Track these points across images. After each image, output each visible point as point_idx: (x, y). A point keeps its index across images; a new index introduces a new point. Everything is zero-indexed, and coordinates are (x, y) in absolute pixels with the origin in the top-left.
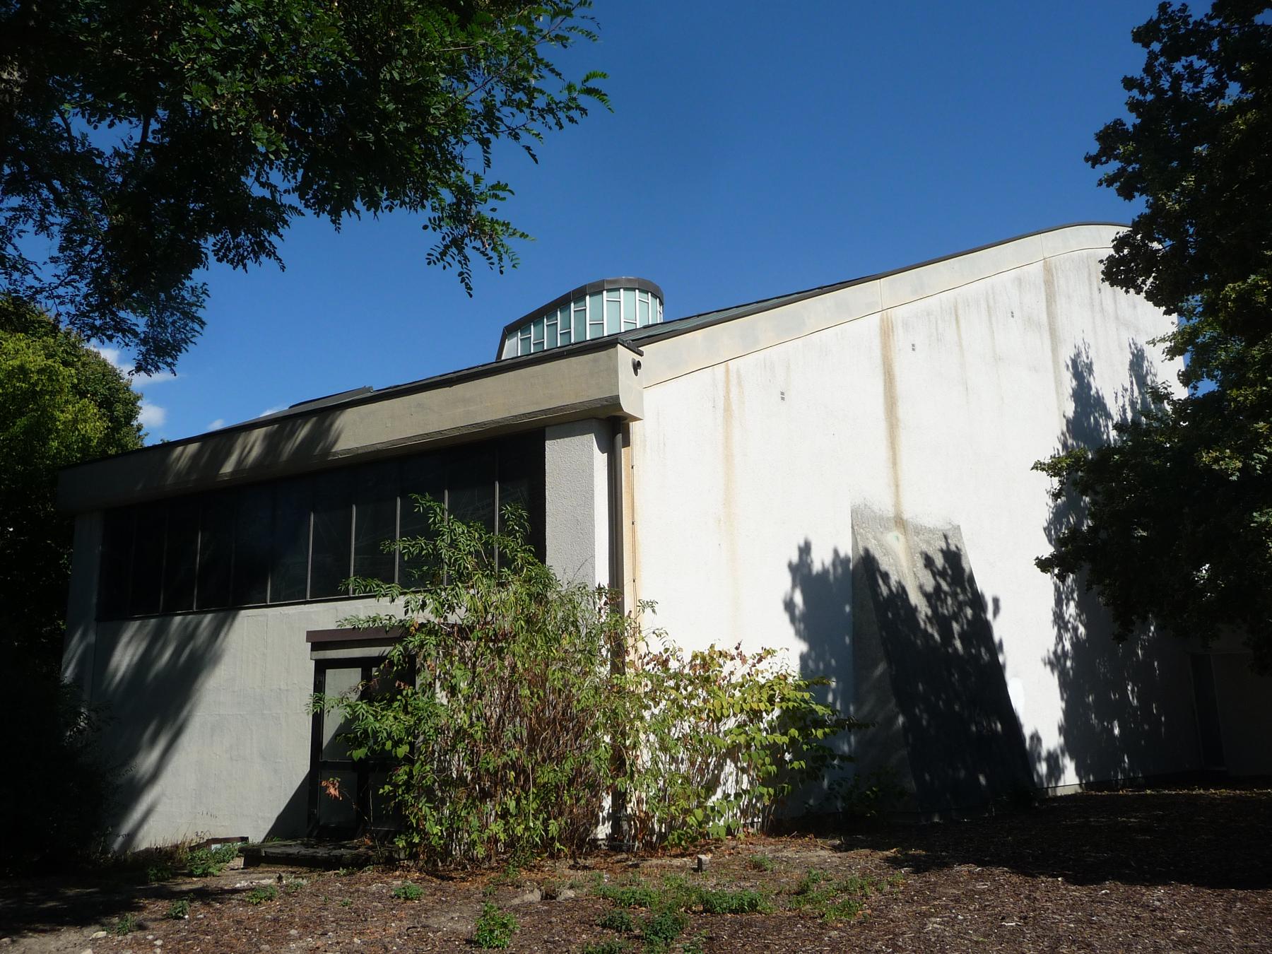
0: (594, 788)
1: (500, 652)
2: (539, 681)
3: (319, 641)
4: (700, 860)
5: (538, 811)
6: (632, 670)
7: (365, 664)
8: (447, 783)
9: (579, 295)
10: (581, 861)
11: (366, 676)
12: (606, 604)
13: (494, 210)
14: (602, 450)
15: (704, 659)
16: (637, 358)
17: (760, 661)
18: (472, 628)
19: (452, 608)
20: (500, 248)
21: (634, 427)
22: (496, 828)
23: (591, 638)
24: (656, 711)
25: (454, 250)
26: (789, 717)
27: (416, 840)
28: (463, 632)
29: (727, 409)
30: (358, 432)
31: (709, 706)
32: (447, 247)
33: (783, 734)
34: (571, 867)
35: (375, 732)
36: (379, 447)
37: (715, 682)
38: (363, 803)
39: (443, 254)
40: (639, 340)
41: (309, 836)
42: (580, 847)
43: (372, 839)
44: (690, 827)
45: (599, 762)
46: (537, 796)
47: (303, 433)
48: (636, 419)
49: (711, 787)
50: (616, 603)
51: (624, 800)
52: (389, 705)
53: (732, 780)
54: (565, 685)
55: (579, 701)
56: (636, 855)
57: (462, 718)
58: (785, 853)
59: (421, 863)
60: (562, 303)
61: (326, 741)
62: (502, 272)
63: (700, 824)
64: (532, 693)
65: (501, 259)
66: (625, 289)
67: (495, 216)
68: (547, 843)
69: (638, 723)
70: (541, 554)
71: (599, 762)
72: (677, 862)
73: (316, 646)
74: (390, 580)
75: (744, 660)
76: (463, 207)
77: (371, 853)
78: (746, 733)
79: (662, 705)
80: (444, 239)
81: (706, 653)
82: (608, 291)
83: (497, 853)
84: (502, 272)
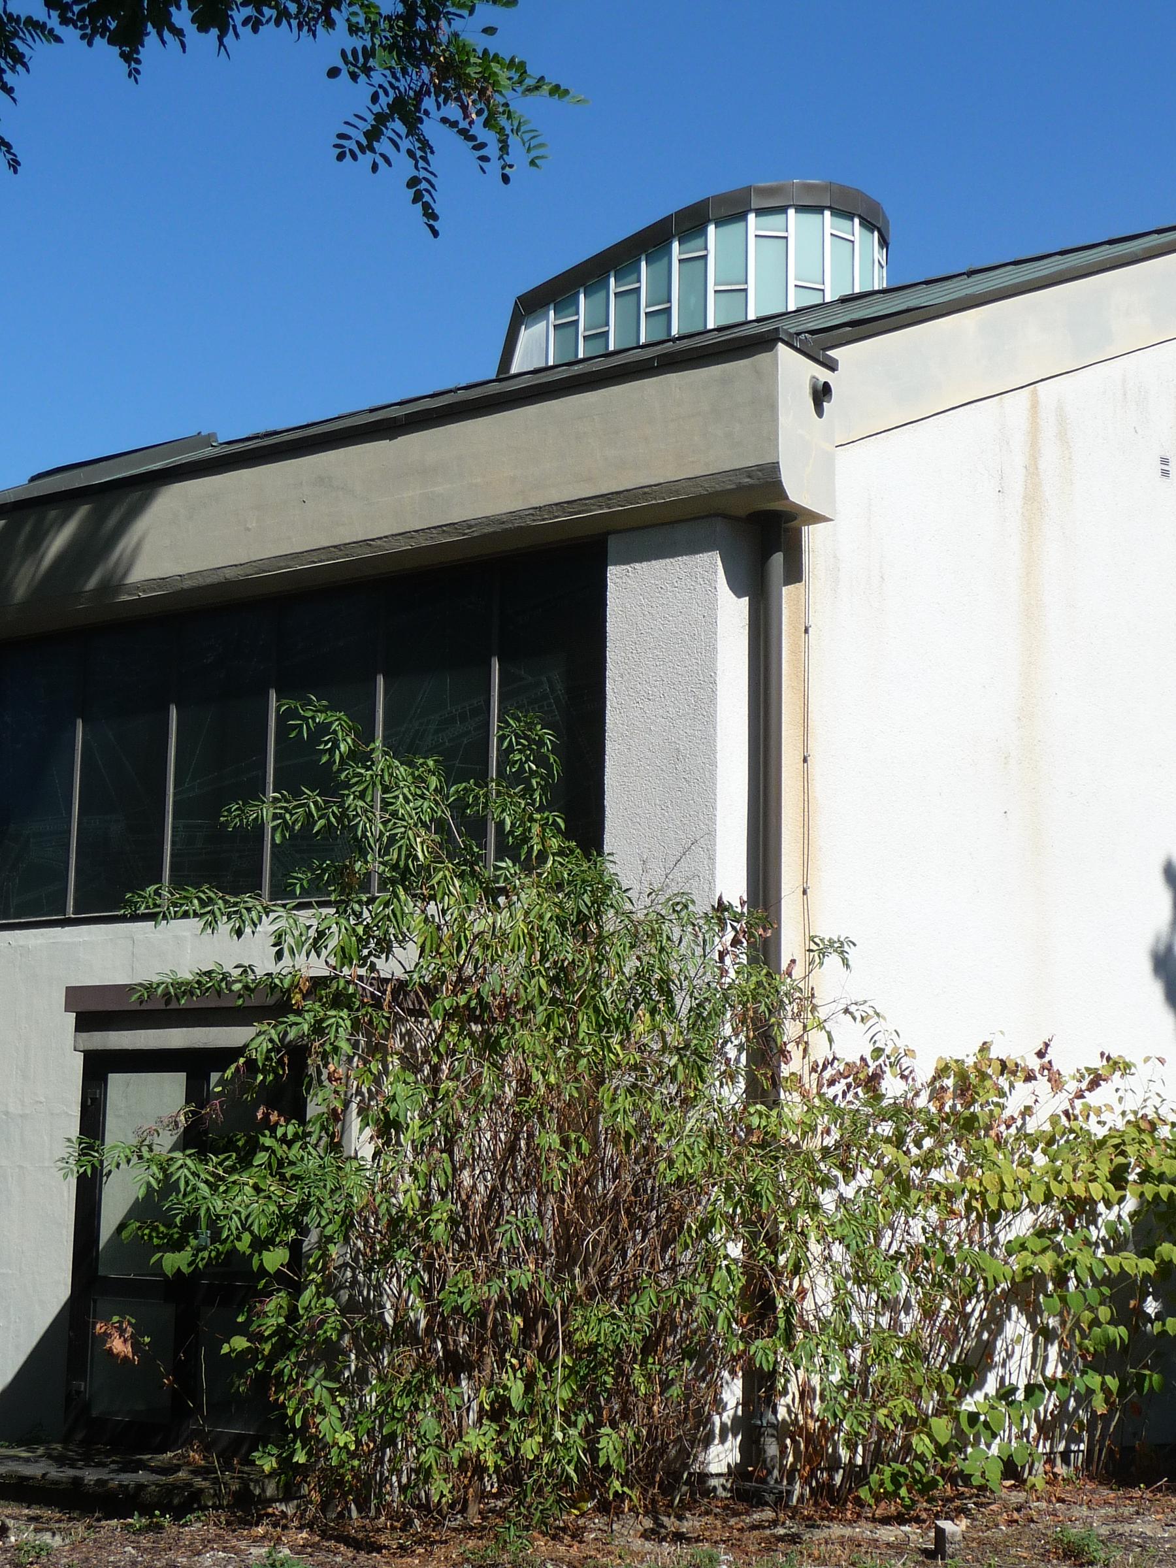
0: (702, 1355)
1: (489, 1046)
2: (581, 1118)
3: (94, 1010)
4: (940, 1532)
5: (572, 1408)
6: (796, 1098)
7: (195, 1065)
8: (373, 1339)
9: (691, 222)
10: (670, 1523)
11: (196, 1093)
12: (735, 942)
13: (489, 31)
14: (738, 592)
15: (963, 1076)
16: (823, 375)
17: (1094, 1084)
18: (431, 992)
19: (385, 947)
20: (503, 121)
21: (813, 537)
22: (479, 1439)
23: (701, 1019)
24: (849, 1191)
25: (398, 125)
26: (1162, 1217)
27: (300, 1458)
28: (410, 998)
29: (1032, 497)
30: (180, 542)
31: (972, 1184)
32: (381, 119)
33: (1141, 1254)
34: (645, 1535)
35: (214, 1222)
36: (230, 574)
37: (989, 1128)
38: (185, 1373)
39: (373, 135)
40: (827, 331)
41: (66, 1440)
42: (667, 1490)
43: (206, 1449)
44: (921, 1458)
45: (718, 1301)
46: (573, 1371)
47: (59, 542)
48: (815, 518)
49: (970, 1371)
50: (764, 951)
51: (772, 1387)
52: (245, 1162)
53: (1018, 1353)
54: (640, 1129)
55: (671, 1163)
56: (795, 1513)
57: (407, 1193)
58: (1139, 1526)
59: (312, 1510)
60: (652, 242)
61: (106, 1232)
62: (506, 179)
63: (942, 1451)
64: (565, 1142)
65: (504, 148)
66: (801, 209)
67: (493, 45)
68: (594, 1476)
69: (803, 1218)
70: (585, 823)
71: (718, 1301)
72: (889, 1534)
73: (87, 1021)
74: (254, 887)
75: (1056, 1082)
76: (421, 24)
77: (199, 1483)
78: (1057, 1249)
79: (863, 1178)
80: (375, 98)
81: (970, 1062)
82: (760, 212)
83: (482, 1495)
84: (506, 179)
